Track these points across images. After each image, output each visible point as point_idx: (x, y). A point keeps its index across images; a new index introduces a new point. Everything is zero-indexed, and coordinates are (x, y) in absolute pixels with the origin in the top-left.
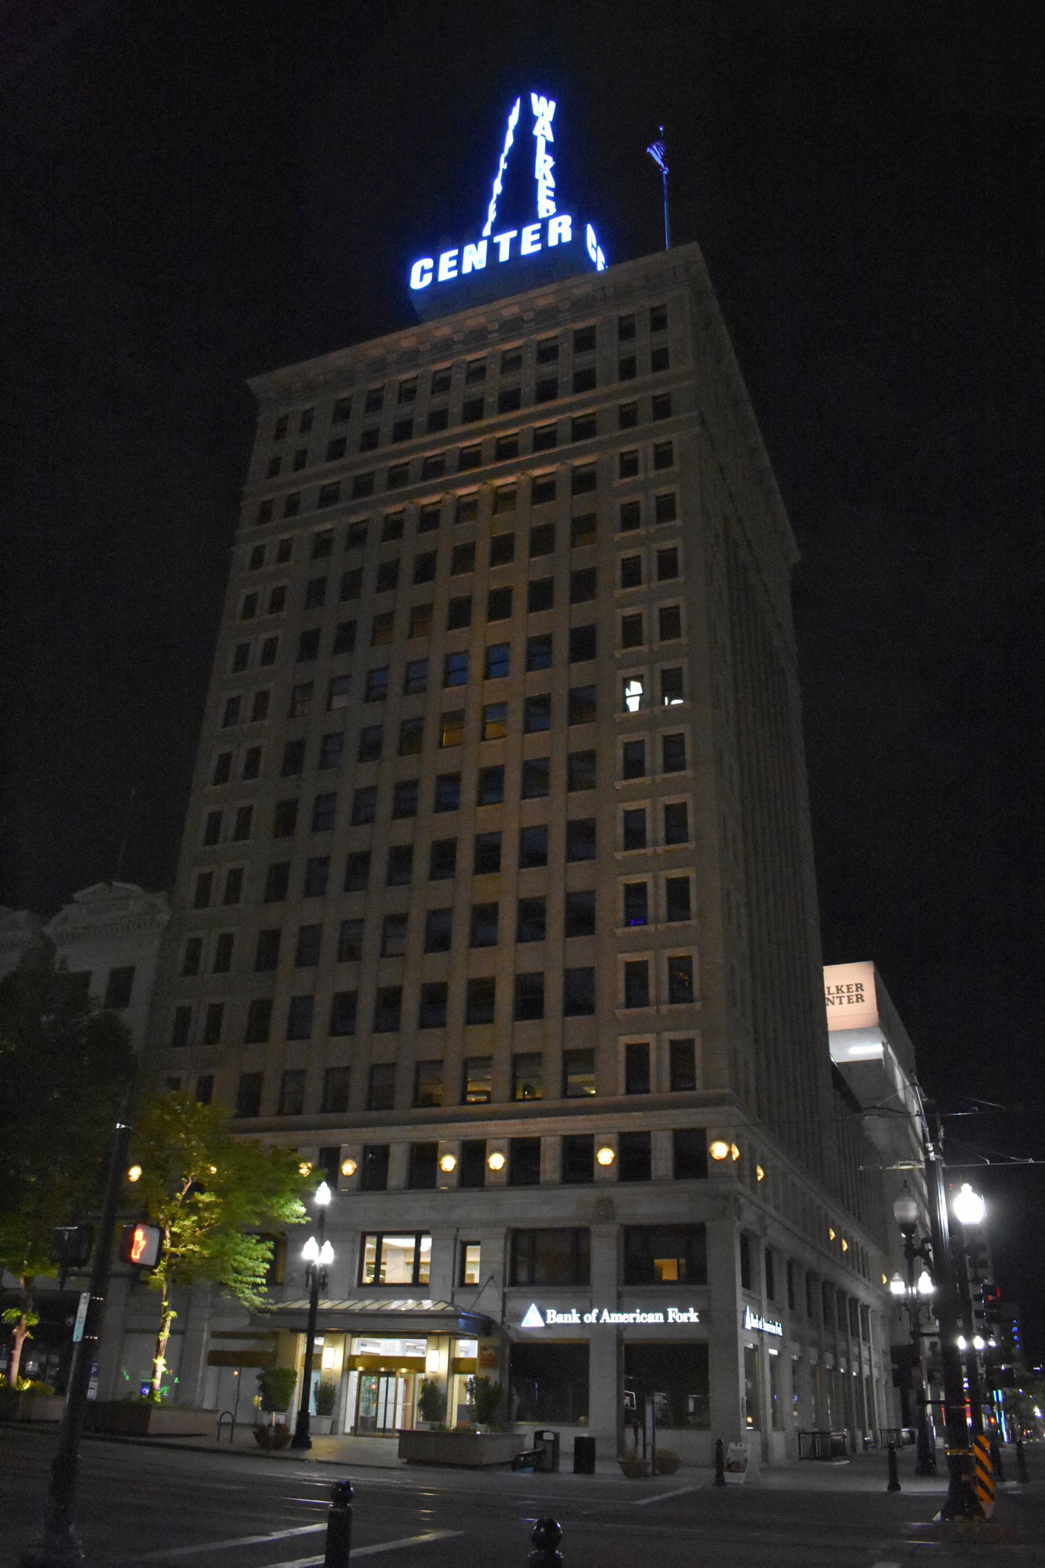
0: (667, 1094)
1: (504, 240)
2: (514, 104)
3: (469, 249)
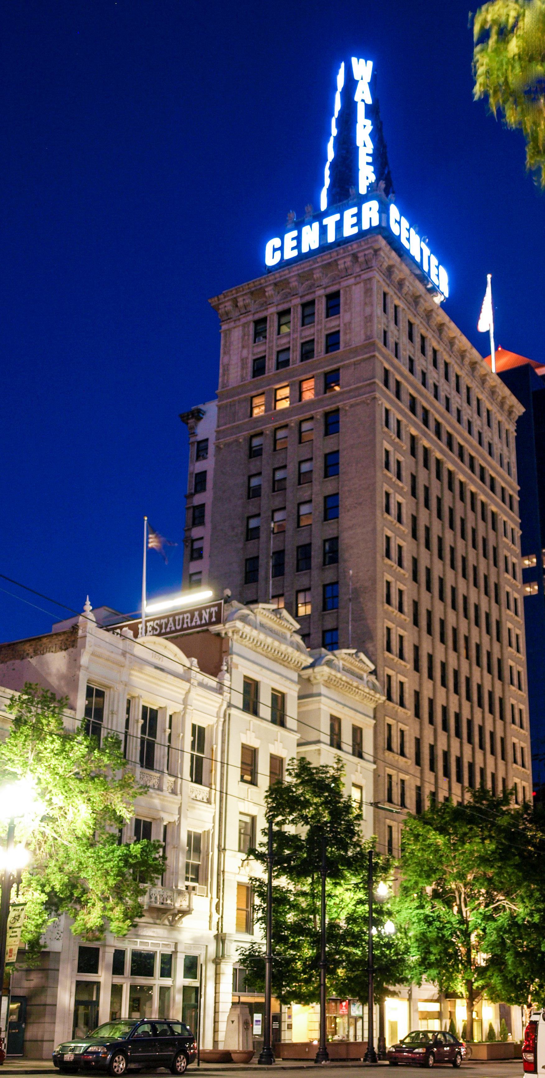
0: (198, 980)
1: (330, 221)
2: (339, 67)
3: (306, 229)
